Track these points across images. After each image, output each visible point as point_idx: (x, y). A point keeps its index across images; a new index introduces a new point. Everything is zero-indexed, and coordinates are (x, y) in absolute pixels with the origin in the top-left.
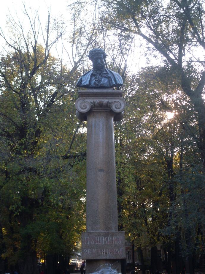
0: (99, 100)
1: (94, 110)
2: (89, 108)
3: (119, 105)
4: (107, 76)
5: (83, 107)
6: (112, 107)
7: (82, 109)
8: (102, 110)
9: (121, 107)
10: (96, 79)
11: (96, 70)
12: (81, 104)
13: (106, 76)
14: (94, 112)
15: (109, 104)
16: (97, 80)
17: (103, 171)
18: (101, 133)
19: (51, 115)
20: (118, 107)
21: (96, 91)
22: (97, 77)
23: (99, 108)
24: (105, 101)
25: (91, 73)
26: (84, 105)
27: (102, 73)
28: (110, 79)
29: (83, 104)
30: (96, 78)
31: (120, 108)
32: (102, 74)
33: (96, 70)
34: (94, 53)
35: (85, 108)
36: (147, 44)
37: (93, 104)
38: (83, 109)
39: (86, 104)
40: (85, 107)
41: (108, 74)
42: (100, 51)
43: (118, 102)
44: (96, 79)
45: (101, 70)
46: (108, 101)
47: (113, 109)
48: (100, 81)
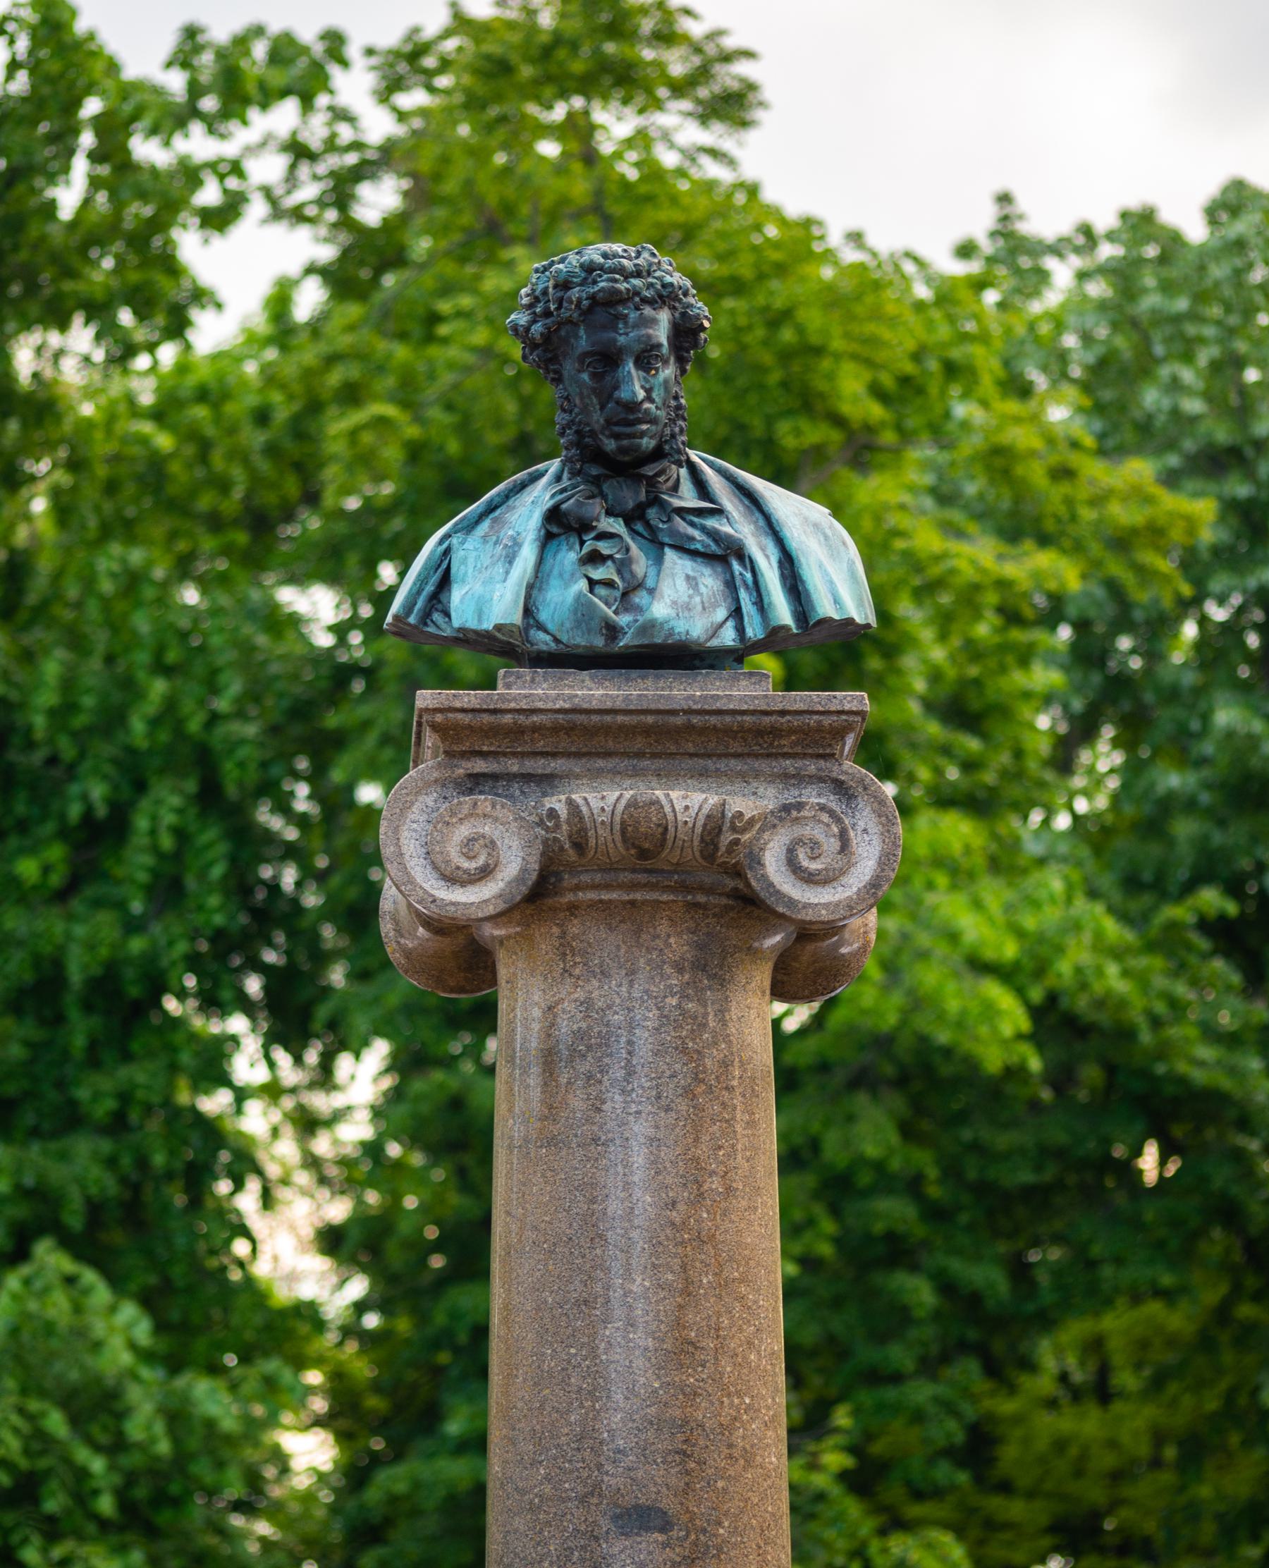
0: (628, 795)
1: (577, 888)
2: (524, 870)
3: (833, 844)
4: (714, 535)
5: (466, 865)
6: (756, 861)
7: (453, 878)
8: (654, 896)
9: (850, 865)
10: (598, 573)
11: (594, 471)
12: (441, 824)
13: (696, 520)
14: (573, 908)
15: (727, 838)
16: (609, 584)
17: (665, 1527)
18: (640, 1129)
19: (513, 384)
20: (814, 866)
21: (590, 691)
22: (604, 548)
23: (626, 877)
24: (687, 801)
25: (547, 502)
26: (471, 840)
27: (655, 501)
28: (736, 567)
29: (464, 831)
30: (595, 558)
31: (843, 872)
32: (652, 513)
33: (594, 471)
34: (575, 293)
35: (485, 873)
36: (370, 52)
37: (563, 835)
38: (463, 884)
39: (487, 829)
40: (481, 861)
41: (719, 512)
42: (638, 274)
43: (823, 808)
44: (598, 573)
45: (650, 470)
46: (713, 800)
47: (765, 877)
48: (629, 592)
